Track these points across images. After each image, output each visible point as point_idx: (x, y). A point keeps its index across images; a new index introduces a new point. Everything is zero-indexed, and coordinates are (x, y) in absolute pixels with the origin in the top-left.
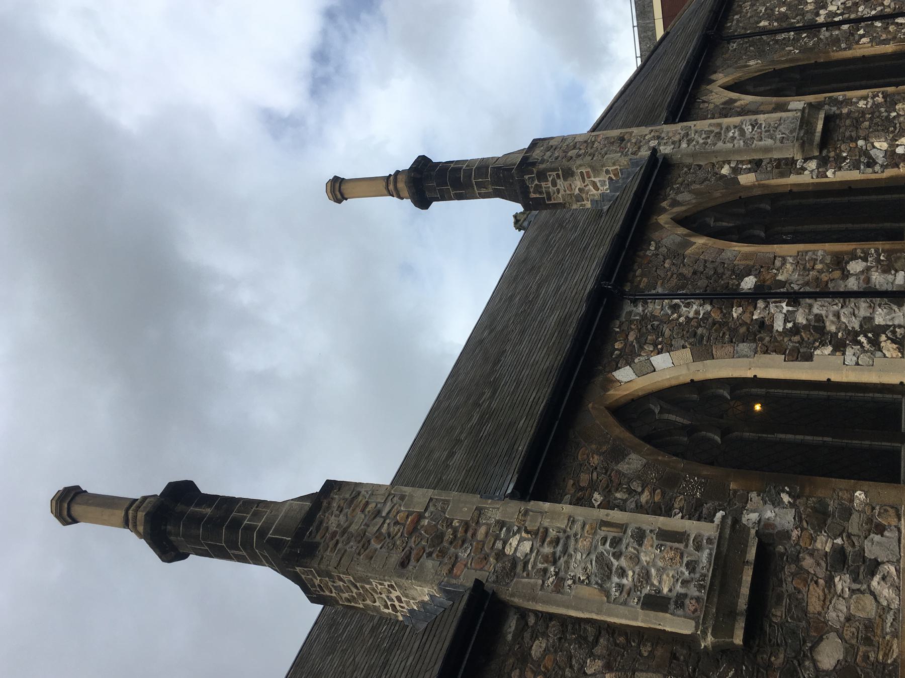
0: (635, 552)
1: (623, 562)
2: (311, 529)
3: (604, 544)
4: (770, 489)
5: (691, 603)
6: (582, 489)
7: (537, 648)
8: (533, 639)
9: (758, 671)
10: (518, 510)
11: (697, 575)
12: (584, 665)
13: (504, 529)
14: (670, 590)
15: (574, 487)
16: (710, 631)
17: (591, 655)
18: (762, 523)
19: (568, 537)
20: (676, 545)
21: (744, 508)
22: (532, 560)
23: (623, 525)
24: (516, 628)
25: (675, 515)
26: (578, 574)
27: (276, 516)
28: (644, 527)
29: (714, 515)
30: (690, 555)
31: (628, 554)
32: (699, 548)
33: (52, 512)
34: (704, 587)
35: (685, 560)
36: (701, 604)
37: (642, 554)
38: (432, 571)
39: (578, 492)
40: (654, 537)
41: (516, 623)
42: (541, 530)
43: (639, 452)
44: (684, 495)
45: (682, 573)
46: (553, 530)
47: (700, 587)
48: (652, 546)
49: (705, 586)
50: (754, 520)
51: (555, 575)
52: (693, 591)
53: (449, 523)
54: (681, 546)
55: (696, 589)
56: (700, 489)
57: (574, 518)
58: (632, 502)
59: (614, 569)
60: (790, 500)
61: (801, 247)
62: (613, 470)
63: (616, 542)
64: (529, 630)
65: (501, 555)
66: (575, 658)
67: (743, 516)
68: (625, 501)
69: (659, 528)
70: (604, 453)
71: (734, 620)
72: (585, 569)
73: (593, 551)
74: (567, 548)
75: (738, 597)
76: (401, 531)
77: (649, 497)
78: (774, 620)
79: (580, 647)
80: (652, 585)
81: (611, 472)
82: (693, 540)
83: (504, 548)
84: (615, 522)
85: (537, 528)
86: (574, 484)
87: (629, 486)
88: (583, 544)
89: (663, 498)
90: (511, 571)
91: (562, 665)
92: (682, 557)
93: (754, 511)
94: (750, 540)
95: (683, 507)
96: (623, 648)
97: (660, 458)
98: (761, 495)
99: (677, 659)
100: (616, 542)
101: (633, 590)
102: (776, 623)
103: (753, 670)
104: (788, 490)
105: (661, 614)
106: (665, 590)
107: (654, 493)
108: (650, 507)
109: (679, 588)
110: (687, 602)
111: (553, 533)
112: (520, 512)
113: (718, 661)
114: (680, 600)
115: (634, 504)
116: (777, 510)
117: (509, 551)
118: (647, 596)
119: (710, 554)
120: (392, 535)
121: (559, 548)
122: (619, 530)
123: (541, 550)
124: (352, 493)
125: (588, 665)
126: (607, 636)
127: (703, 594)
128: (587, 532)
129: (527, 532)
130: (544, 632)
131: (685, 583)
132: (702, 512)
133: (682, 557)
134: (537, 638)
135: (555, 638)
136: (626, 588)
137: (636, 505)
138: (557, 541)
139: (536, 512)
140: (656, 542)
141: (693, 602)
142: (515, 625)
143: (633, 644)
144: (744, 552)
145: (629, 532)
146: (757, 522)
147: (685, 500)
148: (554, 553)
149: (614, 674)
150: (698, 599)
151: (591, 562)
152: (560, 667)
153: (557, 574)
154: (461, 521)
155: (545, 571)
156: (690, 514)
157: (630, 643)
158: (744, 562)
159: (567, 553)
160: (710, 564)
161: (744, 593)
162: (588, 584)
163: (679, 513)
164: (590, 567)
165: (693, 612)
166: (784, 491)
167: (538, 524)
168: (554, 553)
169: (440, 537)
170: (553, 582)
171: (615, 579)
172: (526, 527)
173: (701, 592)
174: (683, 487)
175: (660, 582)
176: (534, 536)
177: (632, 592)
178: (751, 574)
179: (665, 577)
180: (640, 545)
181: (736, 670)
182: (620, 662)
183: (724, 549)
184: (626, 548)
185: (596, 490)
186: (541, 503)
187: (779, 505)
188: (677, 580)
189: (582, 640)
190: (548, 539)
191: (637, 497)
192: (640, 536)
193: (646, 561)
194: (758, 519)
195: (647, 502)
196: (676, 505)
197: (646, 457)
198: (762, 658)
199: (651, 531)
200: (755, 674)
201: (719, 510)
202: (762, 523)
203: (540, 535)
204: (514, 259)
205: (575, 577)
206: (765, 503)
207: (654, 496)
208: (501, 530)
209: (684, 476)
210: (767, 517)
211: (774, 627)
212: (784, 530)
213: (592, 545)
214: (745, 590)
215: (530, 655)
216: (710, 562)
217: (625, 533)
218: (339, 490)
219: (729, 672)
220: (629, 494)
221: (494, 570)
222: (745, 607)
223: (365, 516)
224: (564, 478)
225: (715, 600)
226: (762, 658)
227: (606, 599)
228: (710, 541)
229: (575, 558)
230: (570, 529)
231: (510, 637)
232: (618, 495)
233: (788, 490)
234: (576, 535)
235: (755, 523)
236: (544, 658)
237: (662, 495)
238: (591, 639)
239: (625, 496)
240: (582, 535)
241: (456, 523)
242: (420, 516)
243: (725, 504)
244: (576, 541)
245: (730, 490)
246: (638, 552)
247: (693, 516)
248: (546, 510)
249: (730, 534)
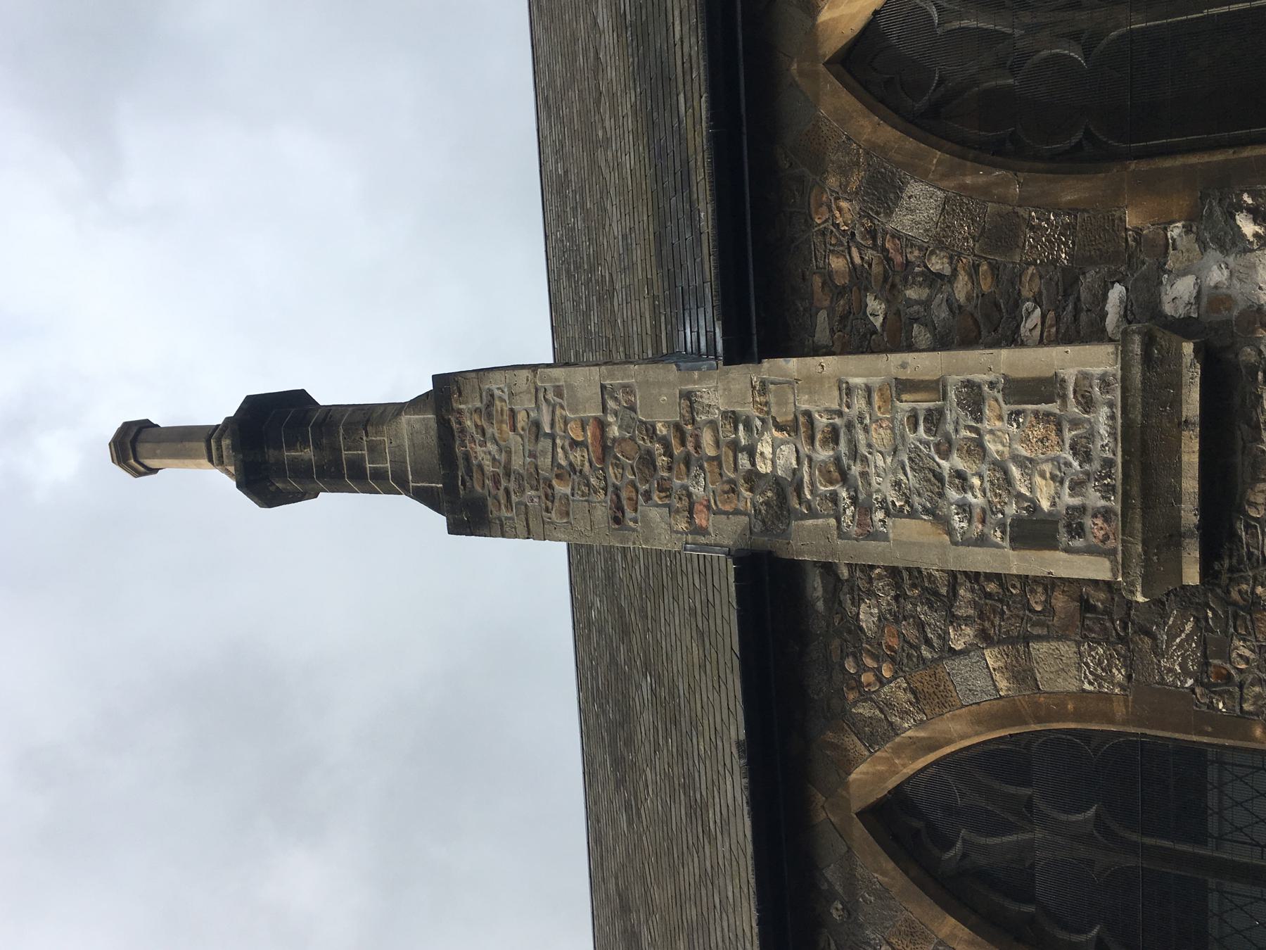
0: (974, 435)
1: (958, 462)
2: (460, 474)
3: (915, 428)
4: (1211, 208)
5: (1094, 524)
6: (841, 292)
7: (867, 616)
8: (856, 604)
9: (1236, 616)
10: (749, 385)
11: (1096, 465)
12: (947, 637)
13: (741, 427)
14: (1054, 504)
15: (826, 289)
16: (1139, 589)
17: (953, 619)
18: (1204, 300)
19: (850, 426)
20: (1043, 407)
21: (1161, 268)
22: (806, 478)
23: (937, 381)
24: (825, 590)
25: (1029, 314)
26: (888, 496)
27: (400, 447)
28: (977, 377)
29: (1105, 297)
30: (1075, 423)
31: (962, 443)
32: (1087, 403)
33: (113, 461)
34: (1112, 489)
35: (1068, 435)
36: (1113, 524)
37: (987, 437)
38: (663, 525)
39: (838, 301)
40: (1000, 396)
41: (822, 582)
42: (801, 419)
43: (923, 176)
44: (1035, 264)
45: (1068, 465)
46: (821, 417)
47: (1107, 490)
48: (1000, 418)
49: (1114, 486)
50: (1186, 298)
51: (852, 503)
52: (1094, 498)
53: (651, 431)
54: (1053, 408)
55: (1098, 494)
56: (1066, 244)
57: (847, 383)
58: (940, 305)
59: (946, 475)
60: (1257, 228)
61: (1119, 404)
62: (885, 232)
63: (934, 419)
64: (845, 589)
65: (753, 478)
66: (929, 626)
67: (1163, 289)
68: (926, 304)
69: (1005, 376)
70: (857, 193)
71: (1179, 545)
72: (897, 484)
73: (900, 447)
74: (855, 446)
75: (1179, 500)
76: (586, 456)
77: (970, 285)
78: (1253, 513)
79: (931, 607)
80: (1020, 496)
81: (884, 240)
82: (1075, 392)
83: (753, 464)
84: (921, 378)
85: (793, 416)
86: (824, 283)
87: (926, 266)
88: (880, 436)
89: (998, 282)
90: (781, 508)
91: (914, 641)
92: (1061, 431)
93: (1184, 273)
94: (1184, 371)
95: (1040, 293)
96: (1001, 601)
97: (968, 180)
98: (1194, 229)
99: (1093, 609)
100: (934, 419)
101: (989, 512)
102: (1256, 519)
103: (1227, 617)
104: (1250, 201)
105: (1047, 554)
106: (1045, 505)
107: (977, 272)
108: (976, 307)
109: (1068, 499)
110: (1088, 522)
111: (822, 421)
112: (754, 388)
113: (1163, 604)
114: (1074, 522)
115: (944, 306)
116: (1231, 260)
117: (764, 468)
118: (1017, 522)
119: (1112, 417)
120: (578, 468)
121: (843, 447)
122: (934, 396)
123: (814, 456)
124: (481, 397)
125: (952, 637)
126: (968, 584)
127: (1115, 503)
128: (879, 408)
129: (780, 428)
130: (869, 590)
131: (1076, 487)
132: (1078, 299)
133: (1059, 431)
134: (861, 600)
135: (889, 598)
136: (977, 512)
137: (951, 310)
138: (833, 436)
139: (780, 383)
140: (1006, 408)
141: (1099, 522)
142: (820, 585)
143: (1014, 592)
144: (1177, 402)
145: (952, 395)
146: (1192, 301)
147: (1041, 277)
148: (837, 460)
149: (996, 649)
150: (1106, 514)
151: (903, 468)
152: (911, 646)
153: (854, 500)
154: (667, 425)
155: (834, 498)
156: (1058, 307)
157: (1009, 590)
158: (1180, 424)
159: (858, 456)
160: (1116, 439)
161: (1189, 463)
162: (913, 515)
163: (1035, 308)
164: (903, 478)
165: (1103, 541)
166: (1240, 207)
167: (791, 408)
168: (837, 460)
169: (648, 460)
170: (853, 516)
171: (953, 495)
172: (774, 419)
173: (1110, 500)
174: (1031, 247)
175: (1031, 490)
176: (792, 434)
177: (988, 516)
178: (1197, 448)
179: (1038, 479)
180: (979, 420)
181: (1197, 620)
182: (1000, 625)
183: (1137, 416)
184: (957, 431)
185: (866, 289)
186: (781, 361)
187: (1234, 244)
188: (1062, 482)
189: (931, 596)
190: (819, 436)
191: (946, 288)
192: (973, 398)
193: (998, 452)
194: (1194, 295)
195: (969, 298)
196: (1026, 293)
197: (940, 184)
198: (1240, 591)
199: (992, 385)
200: (1231, 623)
201: (1113, 283)
202: (1204, 300)
203: (800, 427)
204: (553, 266)
205: (886, 502)
206: (1204, 247)
207: (979, 283)
208: (736, 429)
209: (1026, 216)
210: (1212, 284)
211: (1256, 527)
212: (1251, 306)
213: (894, 434)
214: (1190, 484)
215: (861, 628)
216: (1115, 433)
217: (944, 398)
218: (460, 395)
219: (1183, 625)
220: (930, 287)
221: (755, 510)
222: (1196, 520)
223: (521, 436)
224: (803, 275)
225: (1138, 526)
226: (1240, 591)
227: (947, 538)
228: (1105, 383)
229: (876, 466)
230: (848, 407)
231: (820, 605)
232: (912, 293)
233: (1250, 201)
234: (861, 418)
235: (1189, 303)
236: (883, 631)
237: (993, 274)
238: (944, 591)
239: (924, 293)
240: (873, 418)
241: (661, 429)
242: (602, 425)
243: (1122, 269)
244: (866, 430)
245: (1126, 230)
246: (979, 434)
247: (1064, 308)
248: (796, 375)
249: (1144, 374)
